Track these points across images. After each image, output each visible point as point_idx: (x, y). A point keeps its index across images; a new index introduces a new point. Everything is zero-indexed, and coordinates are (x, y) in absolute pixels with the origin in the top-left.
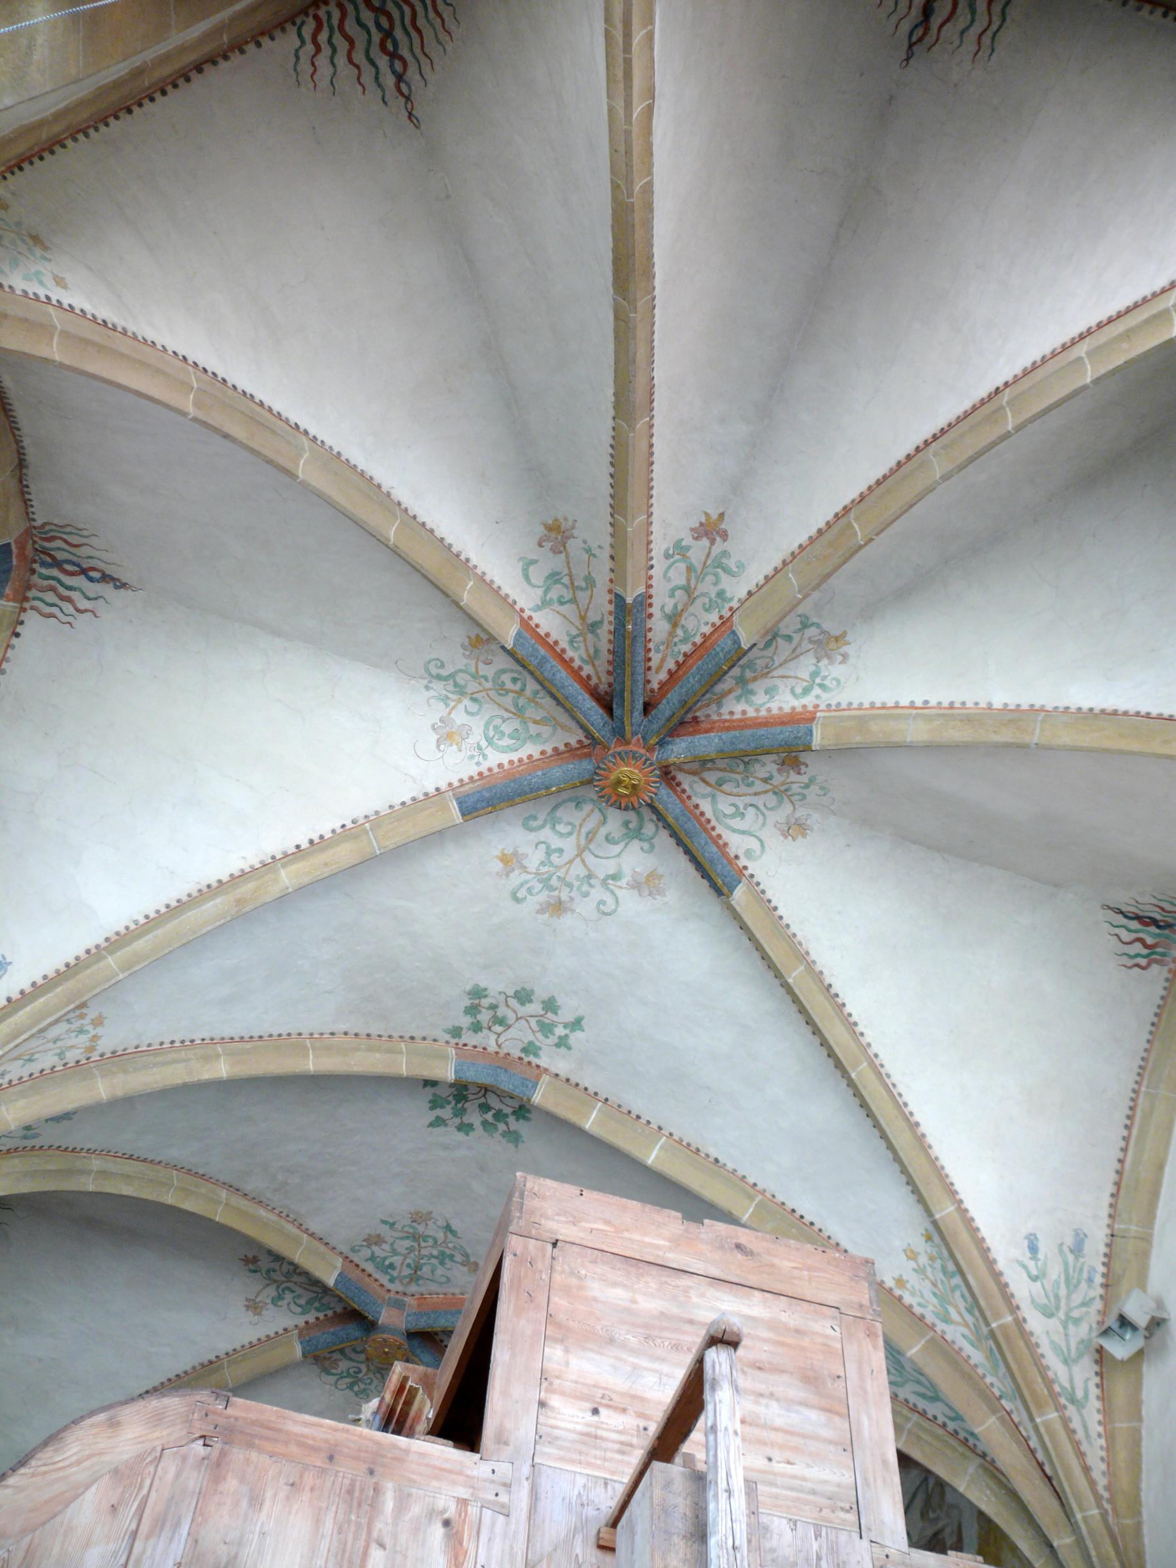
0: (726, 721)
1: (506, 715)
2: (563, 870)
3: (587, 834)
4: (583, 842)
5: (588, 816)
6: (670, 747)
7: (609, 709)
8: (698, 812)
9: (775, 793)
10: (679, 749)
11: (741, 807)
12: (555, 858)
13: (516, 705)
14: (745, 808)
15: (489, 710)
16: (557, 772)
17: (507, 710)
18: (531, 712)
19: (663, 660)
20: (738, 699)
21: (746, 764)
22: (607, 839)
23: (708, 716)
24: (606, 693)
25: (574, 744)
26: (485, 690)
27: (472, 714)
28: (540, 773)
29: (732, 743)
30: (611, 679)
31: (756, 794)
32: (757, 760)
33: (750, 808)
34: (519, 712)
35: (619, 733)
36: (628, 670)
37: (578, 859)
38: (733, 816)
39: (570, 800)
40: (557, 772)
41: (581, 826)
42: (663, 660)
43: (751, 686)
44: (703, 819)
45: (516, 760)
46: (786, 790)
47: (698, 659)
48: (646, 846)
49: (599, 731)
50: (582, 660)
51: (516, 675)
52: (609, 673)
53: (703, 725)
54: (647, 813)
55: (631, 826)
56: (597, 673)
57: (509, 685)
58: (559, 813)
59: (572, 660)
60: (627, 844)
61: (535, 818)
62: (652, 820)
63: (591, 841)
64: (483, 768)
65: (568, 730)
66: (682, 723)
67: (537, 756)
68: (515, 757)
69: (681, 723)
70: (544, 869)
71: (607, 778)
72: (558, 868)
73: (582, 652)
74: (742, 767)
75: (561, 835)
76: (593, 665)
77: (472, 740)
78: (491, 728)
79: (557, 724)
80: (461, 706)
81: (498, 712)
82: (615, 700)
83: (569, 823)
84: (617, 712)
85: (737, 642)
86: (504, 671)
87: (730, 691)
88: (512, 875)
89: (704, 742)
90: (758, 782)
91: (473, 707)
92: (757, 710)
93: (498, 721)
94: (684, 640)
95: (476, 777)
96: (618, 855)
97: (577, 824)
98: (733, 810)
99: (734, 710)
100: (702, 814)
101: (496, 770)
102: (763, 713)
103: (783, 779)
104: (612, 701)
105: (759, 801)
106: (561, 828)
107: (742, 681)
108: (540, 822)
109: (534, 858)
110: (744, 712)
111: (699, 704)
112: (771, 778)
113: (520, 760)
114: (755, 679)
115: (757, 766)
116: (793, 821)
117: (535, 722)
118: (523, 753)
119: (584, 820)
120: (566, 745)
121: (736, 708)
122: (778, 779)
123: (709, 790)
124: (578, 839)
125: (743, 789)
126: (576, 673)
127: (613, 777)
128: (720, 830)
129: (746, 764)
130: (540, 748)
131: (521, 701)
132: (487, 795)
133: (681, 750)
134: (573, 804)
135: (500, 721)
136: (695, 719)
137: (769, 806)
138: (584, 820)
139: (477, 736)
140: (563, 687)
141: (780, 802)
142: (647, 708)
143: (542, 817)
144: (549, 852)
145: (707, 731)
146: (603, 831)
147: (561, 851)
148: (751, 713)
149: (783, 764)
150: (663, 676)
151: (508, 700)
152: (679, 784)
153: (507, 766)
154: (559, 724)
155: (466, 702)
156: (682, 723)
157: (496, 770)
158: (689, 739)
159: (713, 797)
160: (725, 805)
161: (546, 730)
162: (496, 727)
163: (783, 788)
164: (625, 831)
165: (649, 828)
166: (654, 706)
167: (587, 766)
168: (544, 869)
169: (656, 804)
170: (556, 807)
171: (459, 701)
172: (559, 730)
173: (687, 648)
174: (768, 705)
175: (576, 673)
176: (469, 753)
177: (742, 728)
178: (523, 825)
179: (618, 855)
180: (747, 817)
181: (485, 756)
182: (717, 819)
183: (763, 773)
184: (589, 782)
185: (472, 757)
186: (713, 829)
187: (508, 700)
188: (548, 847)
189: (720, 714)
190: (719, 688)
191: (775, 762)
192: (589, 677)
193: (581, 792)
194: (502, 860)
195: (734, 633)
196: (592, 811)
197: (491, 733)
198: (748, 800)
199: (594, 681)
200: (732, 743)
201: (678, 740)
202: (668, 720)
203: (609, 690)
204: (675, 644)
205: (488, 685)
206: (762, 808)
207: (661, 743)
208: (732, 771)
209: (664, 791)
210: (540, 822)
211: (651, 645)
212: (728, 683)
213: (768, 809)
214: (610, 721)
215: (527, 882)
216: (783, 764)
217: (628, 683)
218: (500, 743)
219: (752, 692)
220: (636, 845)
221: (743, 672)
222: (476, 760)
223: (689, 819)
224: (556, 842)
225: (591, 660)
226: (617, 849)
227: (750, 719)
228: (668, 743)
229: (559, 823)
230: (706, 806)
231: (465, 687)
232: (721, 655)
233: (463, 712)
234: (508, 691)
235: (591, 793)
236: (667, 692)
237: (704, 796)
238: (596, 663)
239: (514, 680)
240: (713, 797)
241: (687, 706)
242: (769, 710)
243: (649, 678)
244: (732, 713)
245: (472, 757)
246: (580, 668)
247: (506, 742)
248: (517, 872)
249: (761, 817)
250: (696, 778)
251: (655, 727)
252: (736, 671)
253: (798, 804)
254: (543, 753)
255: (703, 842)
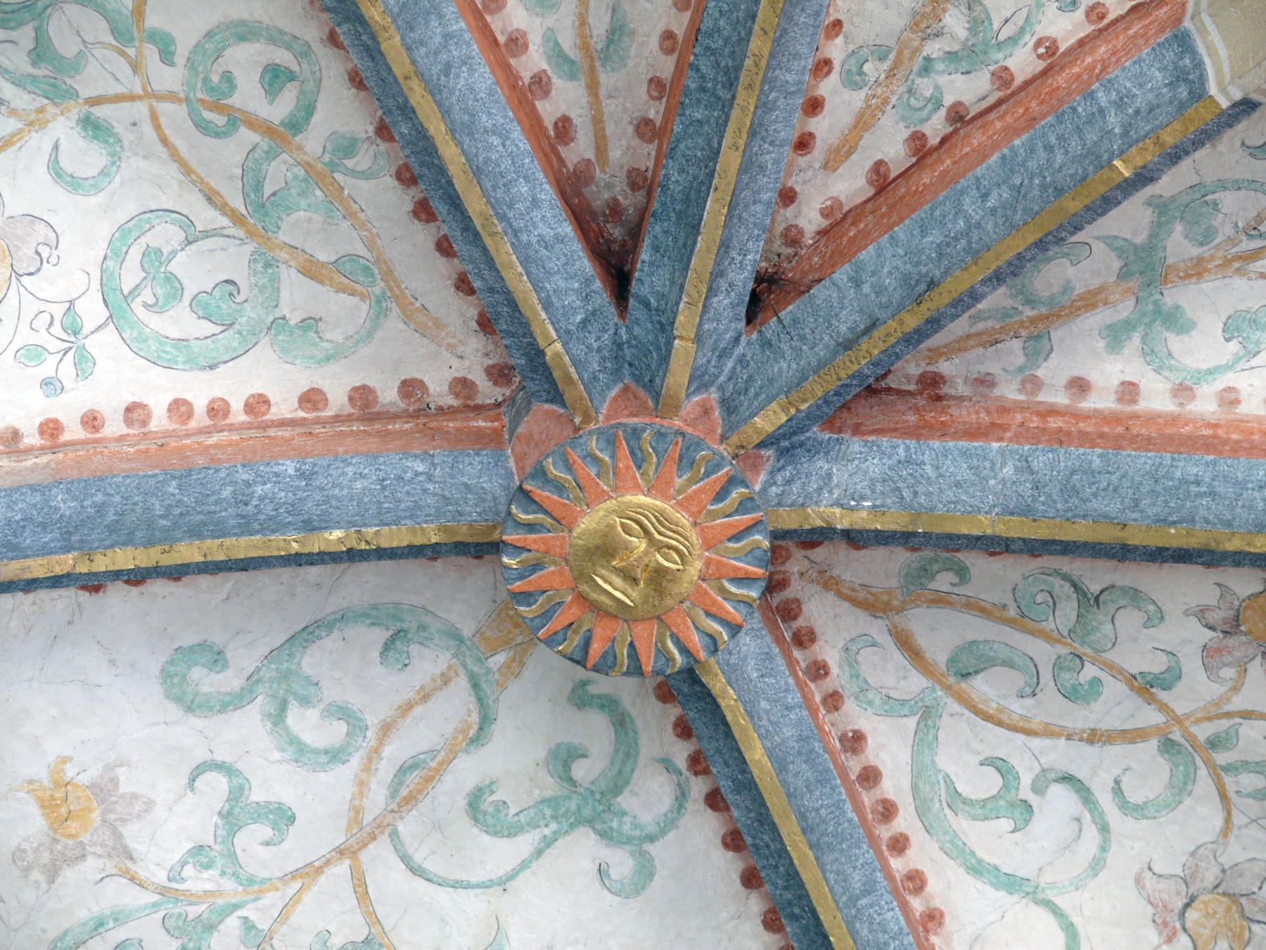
0: (1052, 411)
1: (207, 217)
2: (273, 901)
3: (403, 771)
4: (377, 799)
5: (425, 696)
6: (822, 464)
7: (619, 280)
8: (854, 766)
9: (1168, 746)
10: (855, 479)
11: (1026, 780)
12: (251, 840)
13: (253, 182)
14: (1039, 788)
15: (147, 183)
16: (357, 476)
17: (211, 197)
18: (304, 227)
19: (863, 122)
20: (1116, 336)
21: (1090, 602)
22: (476, 805)
23: (985, 381)
24: (615, 210)
25: (438, 389)
26: (150, 95)
27: (73, 183)
28: (290, 467)
29: (1070, 490)
30: (645, 155)
31: (1093, 737)
32: (1135, 596)
33: (1058, 792)
34: (255, 216)
35: (642, 370)
36: (745, 100)
37: (342, 869)
38: (985, 809)
39: (370, 615)
40: (357, 476)
41: (386, 729)
42: (863, 122)
43: (1177, 296)
44: (868, 799)
45: (200, 405)
46: (1214, 743)
47: (1012, 131)
48: (622, 863)
49: (566, 337)
50: (557, 55)
51: (283, 57)
52: (644, 129)
53: (962, 414)
54: (654, 724)
55: (580, 771)
56: (598, 121)
57: (249, 95)
58: (311, 661)
59: (517, 43)
60: (548, 842)
61: (217, 659)
62: (667, 764)
63: (411, 800)
64: (67, 409)
65: (423, 323)
66: (874, 389)
67: (284, 406)
68: (201, 391)
69: (871, 391)
70: (197, 881)
71: (563, 522)
72: (255, 886)
73: (563, 22)
74: (1068, 610)
75: (300, 752)
76: (593, 87)
77: (53, 286)
78: (135, 254)
79: (389, 296)
80: (39, 143)
81: (173, 192)
82: (654, 231)
83: (343, 712)
84: (649, 277)
85: (1190, 80)
86: (245, 32)
87: (1091, 300)
88: (69, 875)
89: (962, 471)
90: (1114, 688)
91: (84, 156)
92: (1183, 391)
93: (166, 235)
94: (965, 58)
95: (31, 439)
96: (503, 883)
97: (373, 720)
98: (990, 783)
99: (1094, 376)
100: (870, 776)
101: (114, 427)
102: (1205, 405)
103: (1217, 690)
104: (636, 234)
105: (1099, 767)
106: (308, 724)
107: (1145, 269)
108: (230, 680)
109: (171, 828)
110: (1129, 391)
111: (958, 327)
112: (1170, 678)
113: (218, 410)
114: (1197, 270)
115: (1129, 620)
116: (1210, 875)
117: (312, 270)
118: (232, 386)
119: (406, 708)
120: (410, 387)
121: (1100, 368)
122: (1195, 691)
123: (917, 682)
124: (362, 786)
125: (1051, 707)
126: (524, 95)
127: (589, 522)
128: (922, 854)
129: (1090, 602)
130: (305, 379)
131: (279, 173)
132: (64, 505)
133: (862, 486)
134: (379, 636)
135: (177, 235)
136: (932, 384)
137: (1135, 797)
138: (406, 708)
139: (71, 276)
140: (470, 128)
141: (1181, 788)
142: (766, 295)
143: (244, 659)
144: (233, 817)
145: (973, 433)
146: (467, 771)
147: (282, 817)
148: (1156, 398)
149: (1232, 627)
150: (849, 185)
151: (226, 158)
152: (804, 639)
153: (160, 420)
154: (400, 299)
155: (63, 129)
156: (874, 389)
157: (114, 427)
158: (903, 448)
159: (928, 715)
160: (963, 756)
161: (342, 311)
162: (153, 257)
163: (1203, 732)
164: (550, 785)
165: (649, 795)
166: (800, 289)
167: (478, 479)
168: (197, 881)
169: (717, 683)
170: (307, 635)
171: (37, 122)
172: (394, 322)
173: (970, 88)
174: (1228, 379)
175: (524, 95)
176: (25, 336)
177: (1117, 443)
178: (166, 676)
179: (503, 883)
180: (1039, 824)
181: (84, 364)
182: (922, 810)
183: (1140, 658)
184: (483, 549)
185: (33, 353)
186: (899, 844)
187: (226, 158)
188: (237, 794)
189: (1034, 383)
190: (1058, 275)
191: (1201, 613)
192: (564, 127)
193: (415, 586)
194: (48, 805)
195: (1183, 42)
196: (445, 679)
197: (130, 276)
198: (1058, 754)
199: (579, 150)
200: (1070, 490)
201: (856, 445)
202: (847, 345)
203: (630, 201)
204: (926, 69)
205: (168, 78)
206: (1105, 800)
207: (787, 444)
208: (1023, 622)
209: (753, 644)
210: (230, 680)
211: (836, 50)
212: (1087, 264)
213: (1126, 807)
214: (611, 311)
215: (119, 917)
216: (1232, 627)
217: (730, 160)
218: (156, 322)
219: (1174, 320)
220: (582, 850)
221: (1159, 230)
222: (47, 370)
223: (823, 780)
224: (273, 780)
225: (591, 61)
226: (501, 854)
227: (1151, 418)
228: (814, 449)
229: (305, 701)
230: (889, 748)
231: (75, 66)
232: (1114, 121)
233: (41, 171)
234: (238, 119)
235: (461, 599)
236: (863, 240)
237: (892, 706)
238: (606, 79)
239: (275, 77)
240: (928, 715)
241: (932, 307)
242: (1229, 398)
243: (794, 182)
244: (1079, 386)
245: (33, 353)
246: (541, 84)
247: (180, 322)
248: (91, 866)
249: (1091, 835)
250: (877, 629)
251: (784, 368)
252: (1130, 220)
253: (1245, 809)
254: (312, 398)
255: (857, 880)
